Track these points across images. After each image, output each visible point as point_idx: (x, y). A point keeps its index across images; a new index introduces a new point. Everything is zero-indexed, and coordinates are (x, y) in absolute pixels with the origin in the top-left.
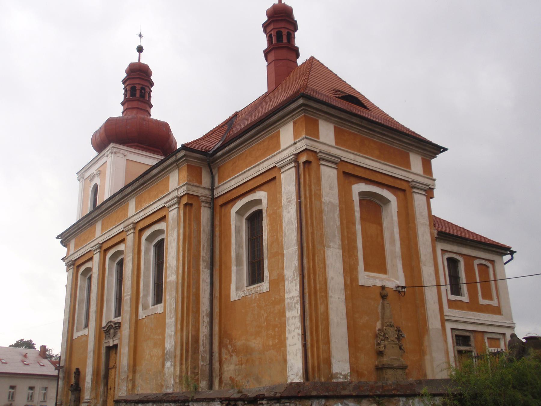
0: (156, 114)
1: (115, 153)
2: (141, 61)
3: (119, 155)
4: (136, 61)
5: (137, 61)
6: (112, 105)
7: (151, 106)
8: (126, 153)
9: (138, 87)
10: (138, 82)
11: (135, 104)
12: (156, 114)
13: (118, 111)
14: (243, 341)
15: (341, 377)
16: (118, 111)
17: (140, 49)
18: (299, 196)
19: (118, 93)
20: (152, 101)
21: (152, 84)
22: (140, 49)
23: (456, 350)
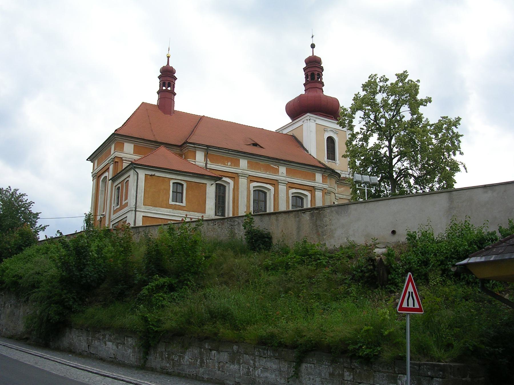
5: (311, 55)
17: (313, 46)
22: (313, 46)
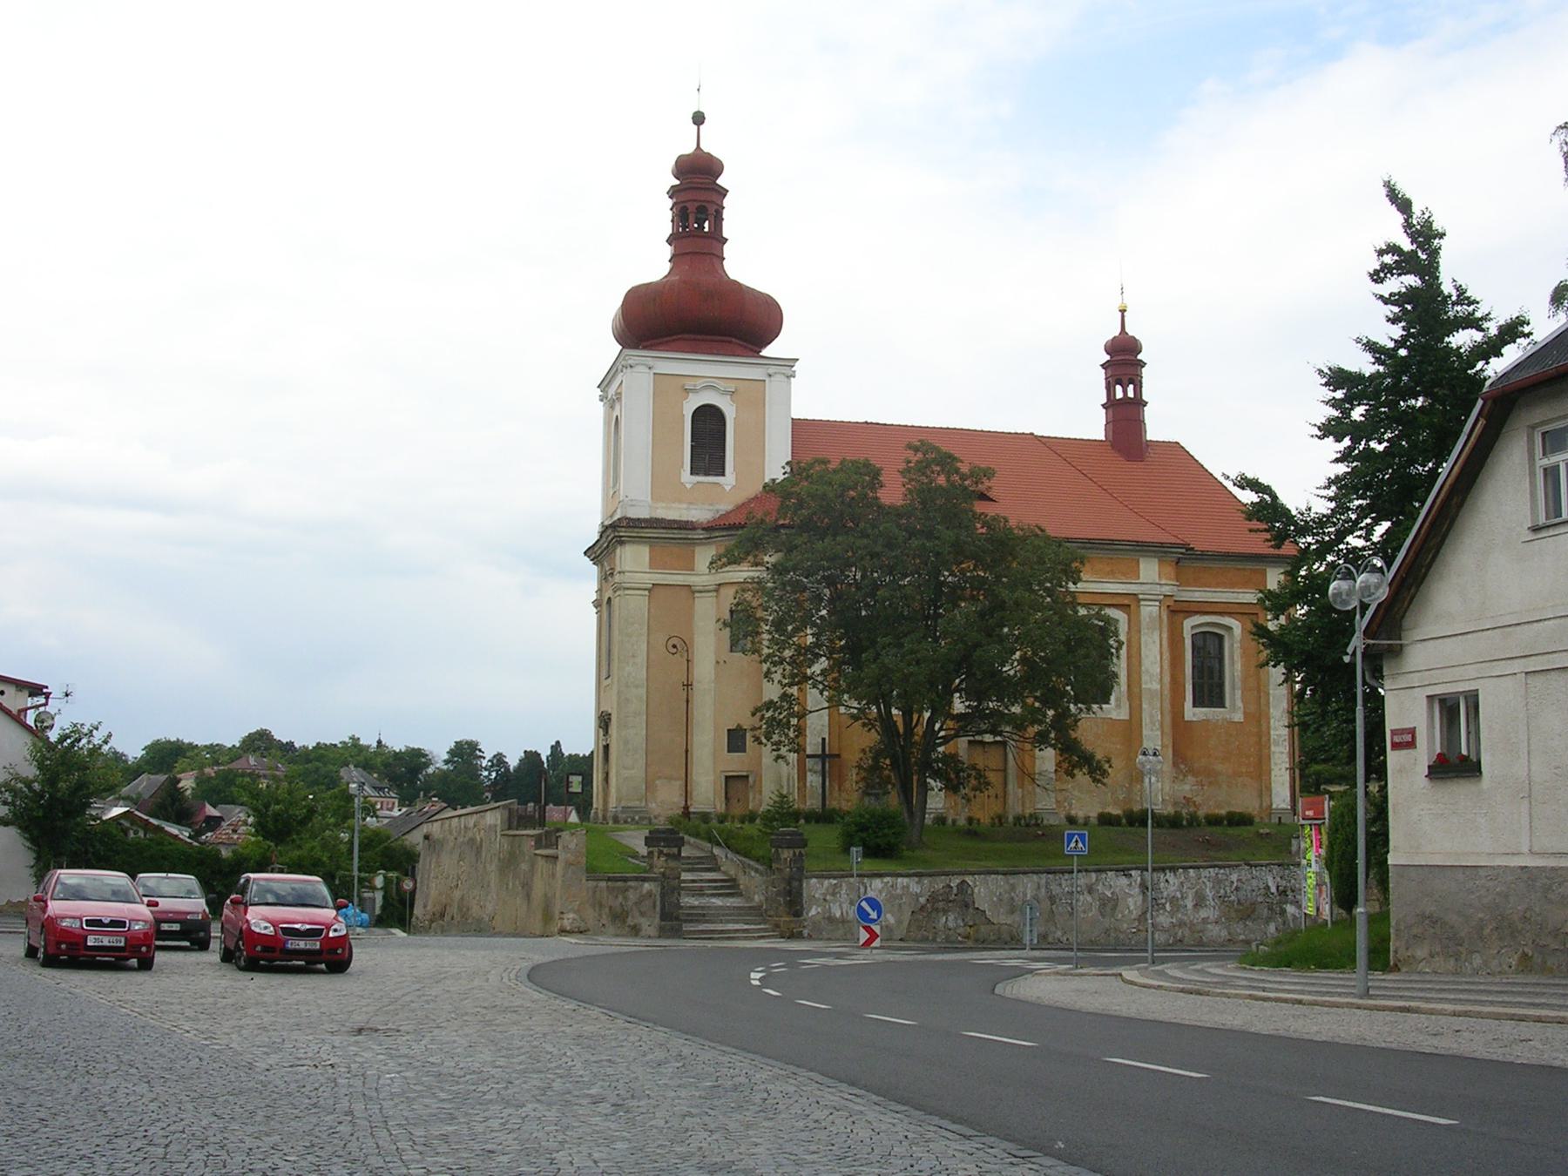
6: (651, 260)
8: (650, 362)
10: (698, 191)
17: (699, 119)
22: (699, 119)
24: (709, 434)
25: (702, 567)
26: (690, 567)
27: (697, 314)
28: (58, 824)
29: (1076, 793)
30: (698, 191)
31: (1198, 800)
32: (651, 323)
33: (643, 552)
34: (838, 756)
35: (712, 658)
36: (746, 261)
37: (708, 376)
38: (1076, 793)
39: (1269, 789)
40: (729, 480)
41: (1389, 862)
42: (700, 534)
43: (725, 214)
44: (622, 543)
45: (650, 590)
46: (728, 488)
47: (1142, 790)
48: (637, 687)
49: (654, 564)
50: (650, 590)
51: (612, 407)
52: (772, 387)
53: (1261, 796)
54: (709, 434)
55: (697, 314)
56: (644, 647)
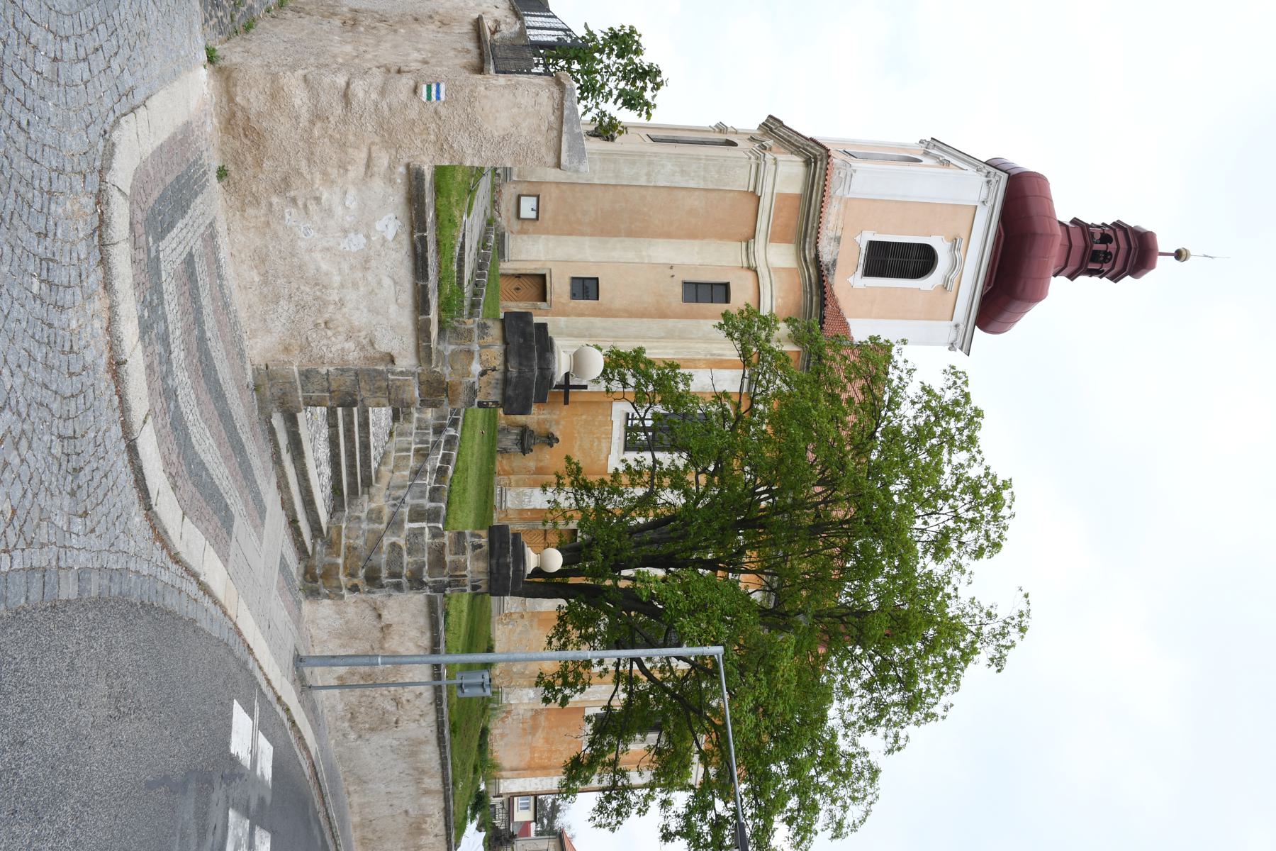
0: (1058, 285)
1: (988, 182)
2: (1160, 258)
3: (985, 190)
4: (1161, 249)
6: (1074, 201)
7: (1072, 277)
8: (989, 204)
9: (1112, 247)
10: (1119, 252)
11: (1078, 242)
12: (1058, 285)
13: (1064, 212)
14: (706, 828)
15: (66, 408)
16: (1064, 212)
17: (1179, 255)
18: (444, 766)
19: (1098, 215)
20: (1083, 280)
21: (1115, 278)
22: (1179, 255)
23: (549, 265)
24: (901, 260)
25: (778, 258)
26: (774, 237)
27: (1026, 248)
28: (709, 839)
29: (519, 629)
30: (1119, 252)
31: (509, 720)
32: (1020, 199)
33: (796, 188)
34: (566, 402)
35: (676, 259)
36: (1069, 304)
37: (965, 265)
38: (519, 629)
39: (518, 777)
40: (861, 282)
41: (507, 598)
42: (810, 255)
43: (1095, 279)
44: (807, 163)
45: (754, 192)
46: (851, 280)
47: (521, 687)
48: (648, 174)
49: (783, 197)
50: (754, 192)
51: (752, 139)
52: (944, 330)
53: (512, 770)
54: (901, 260)
55: (1026, 248)
56: (692, 184)
